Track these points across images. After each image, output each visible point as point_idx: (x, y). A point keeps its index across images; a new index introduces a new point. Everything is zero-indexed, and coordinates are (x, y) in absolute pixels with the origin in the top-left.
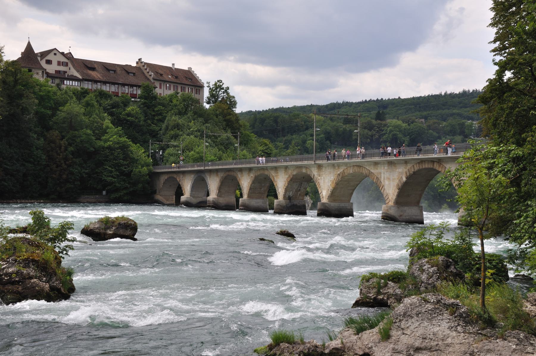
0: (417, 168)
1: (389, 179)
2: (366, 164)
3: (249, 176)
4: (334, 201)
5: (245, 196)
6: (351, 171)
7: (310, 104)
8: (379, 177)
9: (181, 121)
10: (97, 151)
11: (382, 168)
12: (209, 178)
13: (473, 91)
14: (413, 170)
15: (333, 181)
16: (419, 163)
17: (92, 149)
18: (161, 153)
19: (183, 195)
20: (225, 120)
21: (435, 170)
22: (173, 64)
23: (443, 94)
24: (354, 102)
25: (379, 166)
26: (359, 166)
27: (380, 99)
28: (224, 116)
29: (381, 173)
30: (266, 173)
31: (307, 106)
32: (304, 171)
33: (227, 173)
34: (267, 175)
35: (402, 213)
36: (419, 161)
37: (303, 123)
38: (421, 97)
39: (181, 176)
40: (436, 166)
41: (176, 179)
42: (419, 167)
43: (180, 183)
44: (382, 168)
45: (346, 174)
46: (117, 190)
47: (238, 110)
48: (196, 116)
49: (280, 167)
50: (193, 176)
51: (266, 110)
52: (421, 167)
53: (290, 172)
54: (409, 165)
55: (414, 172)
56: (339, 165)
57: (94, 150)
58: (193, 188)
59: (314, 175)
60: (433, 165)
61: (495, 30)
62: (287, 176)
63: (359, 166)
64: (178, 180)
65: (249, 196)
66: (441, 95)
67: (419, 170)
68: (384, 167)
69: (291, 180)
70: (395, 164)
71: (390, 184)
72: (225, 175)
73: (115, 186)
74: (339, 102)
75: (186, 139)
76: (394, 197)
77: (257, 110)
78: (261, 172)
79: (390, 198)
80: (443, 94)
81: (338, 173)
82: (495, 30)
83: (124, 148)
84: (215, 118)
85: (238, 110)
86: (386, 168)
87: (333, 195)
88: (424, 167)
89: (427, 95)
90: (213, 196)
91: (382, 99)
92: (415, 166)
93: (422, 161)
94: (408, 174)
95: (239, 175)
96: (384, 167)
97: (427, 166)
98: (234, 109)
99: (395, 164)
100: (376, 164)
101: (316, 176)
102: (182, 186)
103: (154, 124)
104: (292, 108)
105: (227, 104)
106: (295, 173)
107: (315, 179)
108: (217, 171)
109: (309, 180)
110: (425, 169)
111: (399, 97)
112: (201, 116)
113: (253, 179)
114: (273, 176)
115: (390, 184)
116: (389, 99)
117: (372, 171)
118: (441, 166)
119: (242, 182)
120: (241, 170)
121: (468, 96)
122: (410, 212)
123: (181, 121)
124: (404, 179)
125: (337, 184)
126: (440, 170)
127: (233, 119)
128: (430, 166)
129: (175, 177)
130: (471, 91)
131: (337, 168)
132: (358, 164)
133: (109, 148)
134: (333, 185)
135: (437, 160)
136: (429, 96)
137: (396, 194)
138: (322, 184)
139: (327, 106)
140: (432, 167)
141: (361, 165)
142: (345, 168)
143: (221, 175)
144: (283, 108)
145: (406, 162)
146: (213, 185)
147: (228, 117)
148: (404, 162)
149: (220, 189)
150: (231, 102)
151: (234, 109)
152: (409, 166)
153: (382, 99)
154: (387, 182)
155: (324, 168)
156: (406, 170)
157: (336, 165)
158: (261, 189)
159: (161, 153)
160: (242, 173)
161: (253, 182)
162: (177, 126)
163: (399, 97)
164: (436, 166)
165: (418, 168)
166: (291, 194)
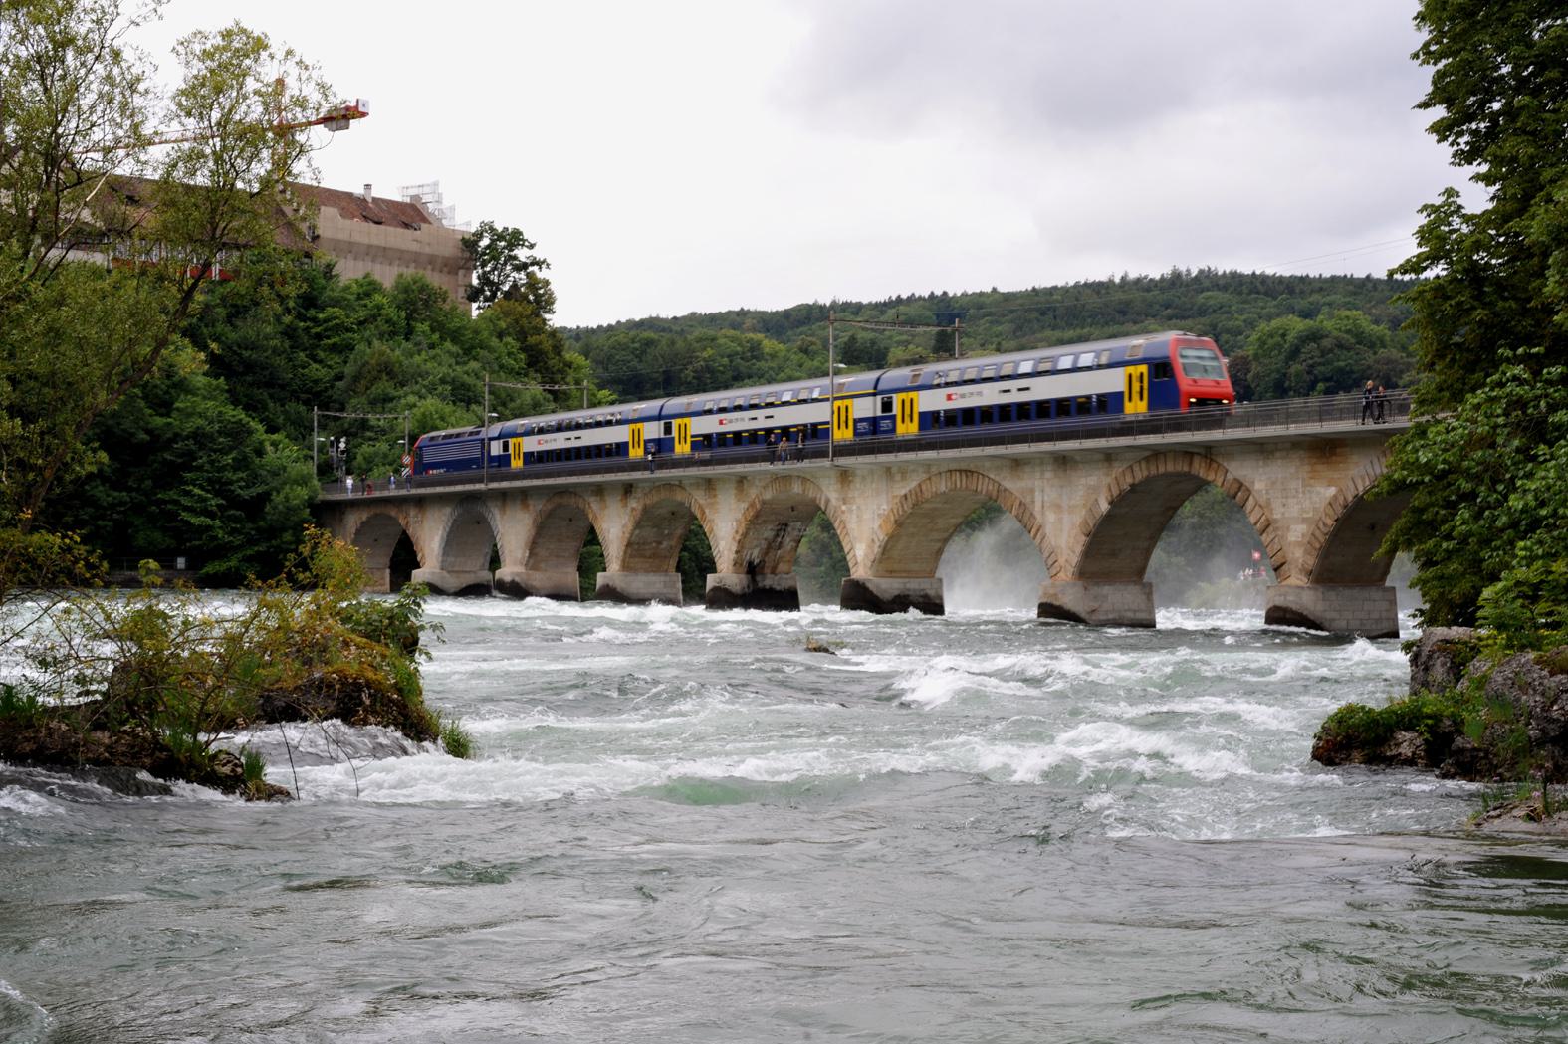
0: (1140, 474)
1: (1058, 507)
2: (987, 464)
3: (626, 505)
4: (891, 573)
5: (614, 566)
6: (942, 486)
7: (737, 308)
8: (1028, 500)
9: (396, 352)
10: (159, 440)
11: (1038, 475)
12: (498, 516)
13: (1201, 271)
14: (1129, 480)
15: (888, 516)
16: (1147, 459)
17: (143, 436)
18: (342, 445)
19: (418, 566)
20: (522, 350)
21: (1197, 477)
22: (368, 187)
23: (1117, 280)
24: (865, 301)
25: (1028, 469)
26: (968, 472)
27: (938, 292)
28: (522, 336)
29: (1032, 491)
30: (679, 496)
31: (729, 312)
32: (797, 488)
33: (557, 500)
34: (682, 504)
35: (1096, 605)
36: (1147, 453)
37: (725, 361)
38: (1055, 288)
39: (412, 512)
40: (1199, 468)
41: (395, 520)
42: (1148, 469)
43: (410, 532)
44: (1038, 475)
45: (927, 495)
46: (221, 552)
47: (560, 318)
48: (436, 337)
49: (721, 478)
50: (448, 510)
51: (610, 327)
52: (1153, 471)
53: (753, 492)
54: (1116, 464)
55: (1132, 485)
56: (904, 471)
57: (146, 437)
58: (451, 544)
59: (828, 501)
60: (1190, 464)
61: (1430, 70)
62: (744, 505)
63: (968, 472)
64: (402, 522)
65: (626, 567)
66: (1111, 281)
67: (1148, 480)
68: (1043, 473)
69: (757, 515)
70: (1076, 462)
71: (1060, 520)
72: (549, 506)
73: (215, 538)
74: (821, 302)
75: (415, 407)
76: (1075, 559)
77: (583, 326)
78: (664, 494)
79: (1062, 561)
80: (1117, 280)
81: (903, 492)
82: (1430, 70)
83: (238, 433)
84: (494, 342)
85: (560, 318)
86: (1048, 474)
87: (886, 557)
88: (1162, 469)
89: (1072, 283)
90: (510, 570)
91: (945, 293)
92: (1136, 468)
93: (1156, 453)
94: (1115, 492)
95: (594, 505)
96: (1043, 473)
97: (1170, 466)
98: (547, 316)
99: (1076, 462)
100: (1017, 463)
101: (834, 501)
102: (414, 540)
103: (315, 361)
104: (684, 318)
105: (529, 301)
106: (768, 495)
107: (830, 513)
108: (523, 495)
109: (813, 513)
110: (1166, 475)
111: (994, 289)
112: (455, 337)
113: (638, 513)
114: (700, 506)
115: (1060, 520)
116: (964, 295)
117: (1007, 484)
118: (1214, 465)
119: (605, 526)
120: (599, 490)
121: (1187, 285)
122: (1120, 598)
123: (396, 352)
124: (1104, 506)
125: (899, 524)
126: (1210, 478)
127: (547, 345)
128: (1181, 466)
129: (393, 513)
130: (1220, 273)
131: (898, 477)
132: (963, 466)
133: (198, 436)
134: (890, 528)
135: (1202, 451)
136: (1077, 285)
137: (1079, 549)
138: (852, 525)
139: (787, 314)
140: (1186, 469)
141: (972, 467)
142: (925, 476)
143: (538, 505)
144: (657, 319)
145: (1108, 456)
146: (513, 532)
147: (532, 340)
148: (1101, 456)
149: (533, 546)
150: (537, 297)
151: (547, 316)
152: (1118, 468)
153: (945, 293)
154: (1051, 517)
155: (858, 480)
156: (1108, 480)
157: (894, 470)
158: (660, 543)
159: (342, 445)
160: (603, 499)
161: (638, 525)
162: (387, 370)
163: (994, 289)
164: (1199, 468)
165: (1145, 473)
166: (755, 555)
